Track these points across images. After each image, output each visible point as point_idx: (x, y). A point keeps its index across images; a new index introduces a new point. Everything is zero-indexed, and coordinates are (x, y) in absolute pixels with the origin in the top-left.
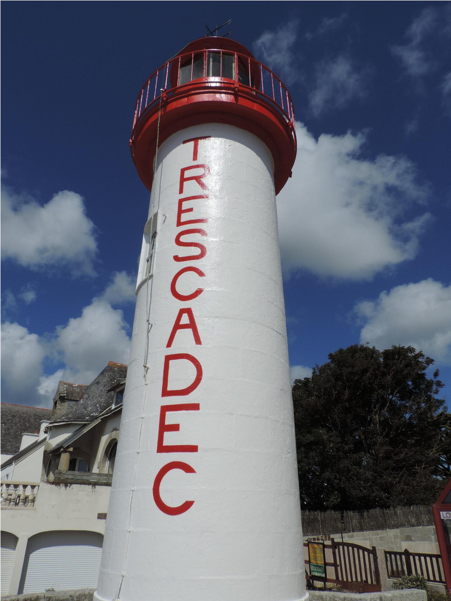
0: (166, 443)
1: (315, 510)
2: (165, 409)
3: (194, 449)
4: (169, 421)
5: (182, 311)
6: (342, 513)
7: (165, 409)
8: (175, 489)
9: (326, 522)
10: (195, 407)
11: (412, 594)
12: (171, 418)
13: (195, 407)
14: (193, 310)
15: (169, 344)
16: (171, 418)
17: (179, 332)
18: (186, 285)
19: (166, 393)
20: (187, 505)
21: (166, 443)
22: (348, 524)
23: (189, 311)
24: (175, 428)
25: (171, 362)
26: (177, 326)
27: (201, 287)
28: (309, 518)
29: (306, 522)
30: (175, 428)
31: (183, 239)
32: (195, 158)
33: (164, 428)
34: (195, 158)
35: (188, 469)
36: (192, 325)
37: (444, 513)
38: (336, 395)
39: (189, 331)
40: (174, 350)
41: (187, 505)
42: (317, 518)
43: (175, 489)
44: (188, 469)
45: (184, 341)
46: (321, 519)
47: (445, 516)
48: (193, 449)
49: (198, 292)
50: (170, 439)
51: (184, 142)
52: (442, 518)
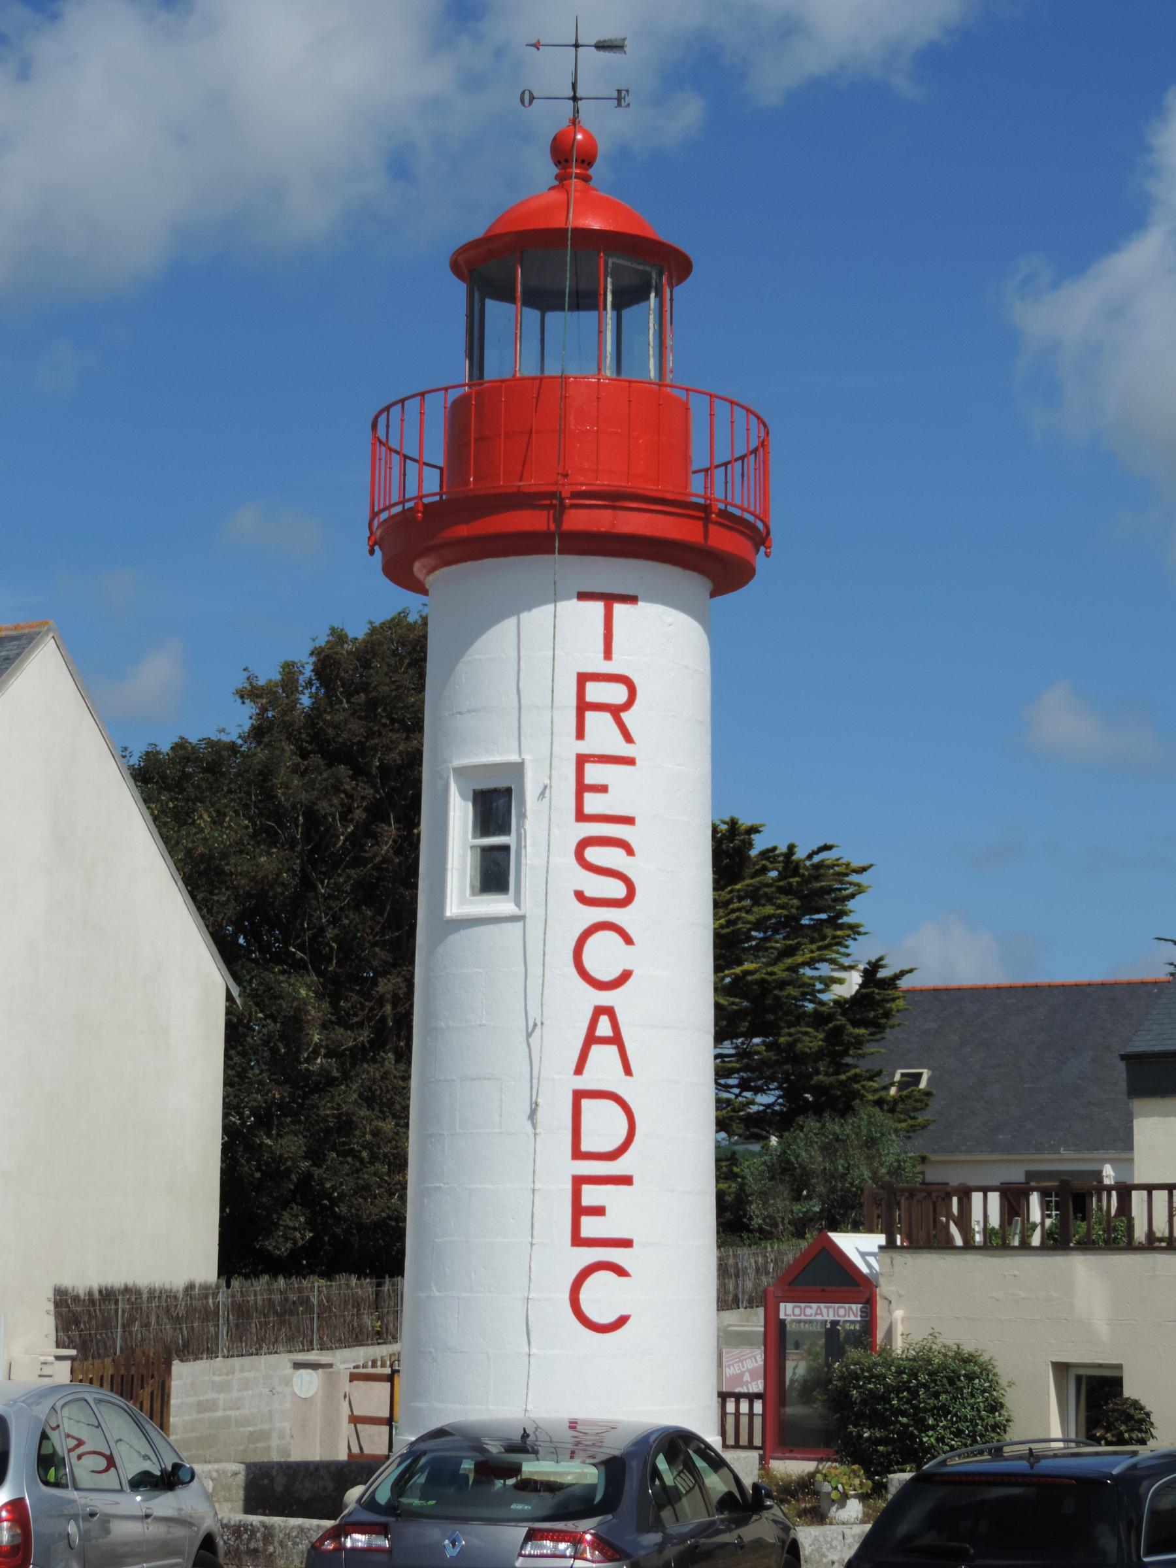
0: (585, 1233)
1: (302, 1273)
2: (579, 1182)
3: (627, 1243)
4: (586, 1201)
5: (599, 1011)
6: (379, 1285)
7: (579, 1182)
8: (601, 1297)
9: (330, 1311)
10: (626, 1180)
11: (739, 1458)
12: (591, 1195)
13: (626, 1180)
14: (617, 1010)
15: (579, 1070)
16: (591, 1195)
17: (596, 1050)
18: (604, 955)
19: (578, 1154)
20: (622, 1321)
21: (585, 1233)
22: (391, 1318)
23: (610, 1012)
24: (599, 1211)
25: (586, 1103)
26: (591, 1039)
27: (629, 968)
28: (286, 1299)
29: (276, 1312)
30: (599, 1211)
31: (594, 855)
32: (608, 654)
33: (579, 1211)
34: (608, 654)
35: (620, 1271)
36: (616, 1039)
37: (790, 1306)
38: (345, 841)
39: (613, 1050)
40: (586, 1082)
41: (622, 1321)
42: (308, 1298)
43: (601, 1297)
44: (620, 1271)
45: (603, 1066)
46: (320, 1302)
47: (789, 1311)
48: (627, 1243)
49: (626, 976)
50: (591, 1227)
51: (583, 596)
52: (782, 1316)
